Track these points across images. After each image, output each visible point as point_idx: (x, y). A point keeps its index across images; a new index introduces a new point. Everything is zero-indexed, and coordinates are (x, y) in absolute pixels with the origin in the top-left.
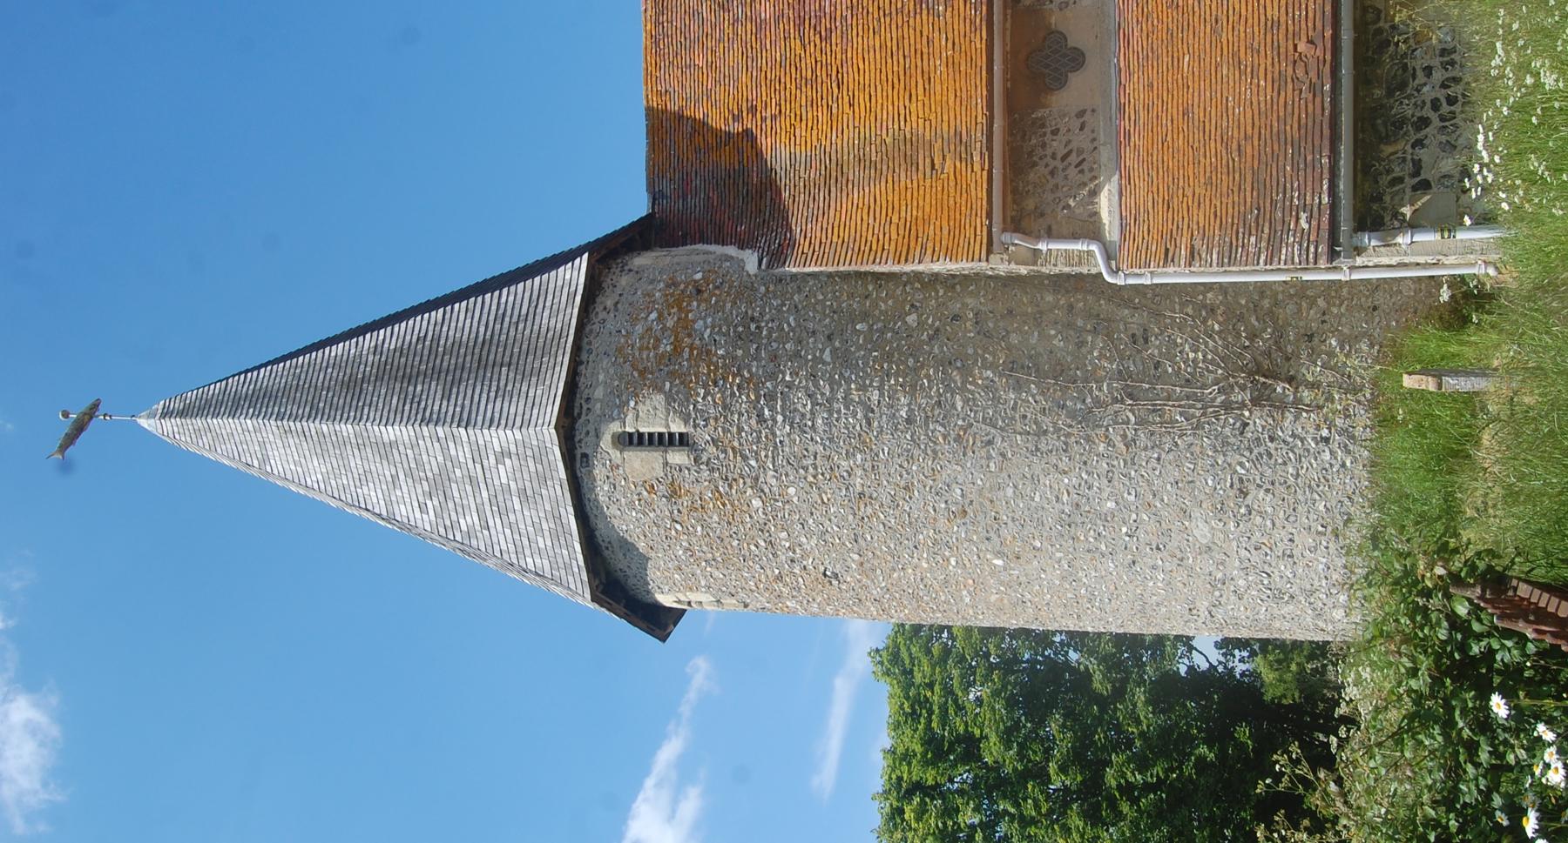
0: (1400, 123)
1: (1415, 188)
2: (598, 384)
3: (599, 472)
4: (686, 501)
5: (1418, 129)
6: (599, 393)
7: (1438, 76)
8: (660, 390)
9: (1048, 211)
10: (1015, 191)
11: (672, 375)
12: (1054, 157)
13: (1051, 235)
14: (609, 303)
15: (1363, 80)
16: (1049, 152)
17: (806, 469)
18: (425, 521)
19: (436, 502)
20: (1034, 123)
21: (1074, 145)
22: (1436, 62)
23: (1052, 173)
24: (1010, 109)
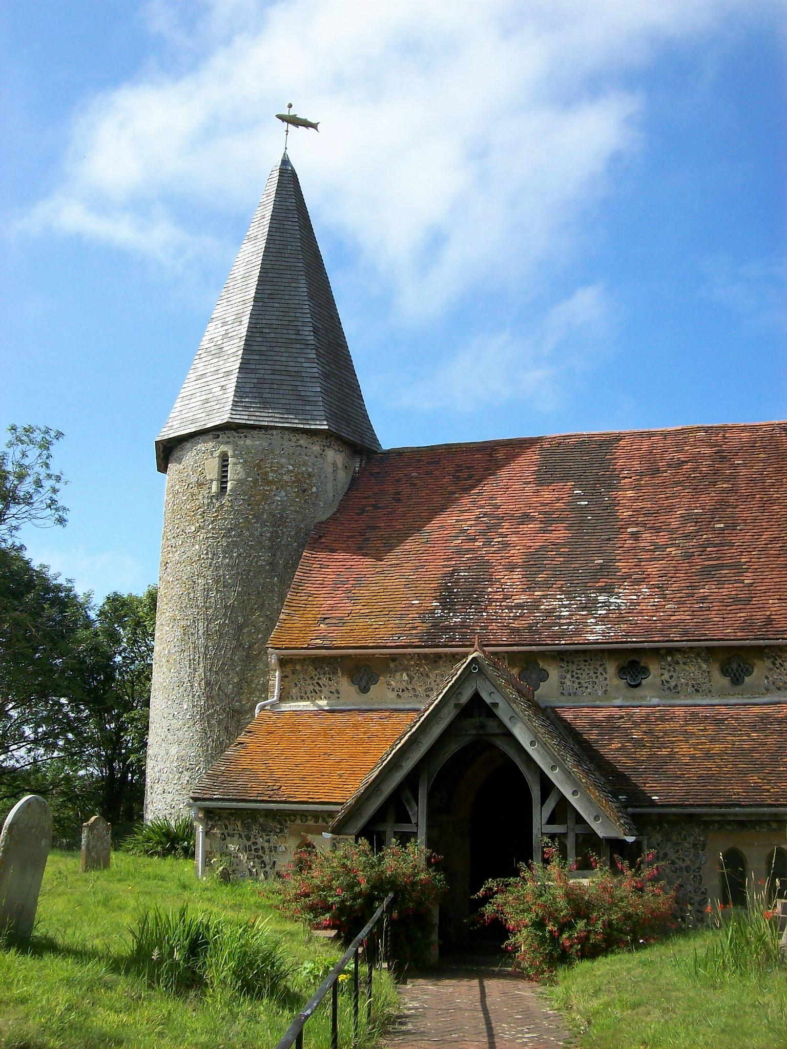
0: (249, 829)
1: (223, 834)
2: (253, 441)
3: (210, 445)
4: (196, 491)
5: (246, 836)
6: (249, 442)
7: (266, 845)
8: (248, 475)
9: (294, 676)
10: (304, 660)
11: (255, 481)
12: (319, 679)
13: (283, 678)
14: (302, 442)
15: (269, 813)
16: (322, 676)
17: (207, 554)
18: (205, 343)
19: (212, 348)
20: (335, 668)
21: (323, 689)
22: (272, 844)
23: (312, 678)
24: (343, 657)
